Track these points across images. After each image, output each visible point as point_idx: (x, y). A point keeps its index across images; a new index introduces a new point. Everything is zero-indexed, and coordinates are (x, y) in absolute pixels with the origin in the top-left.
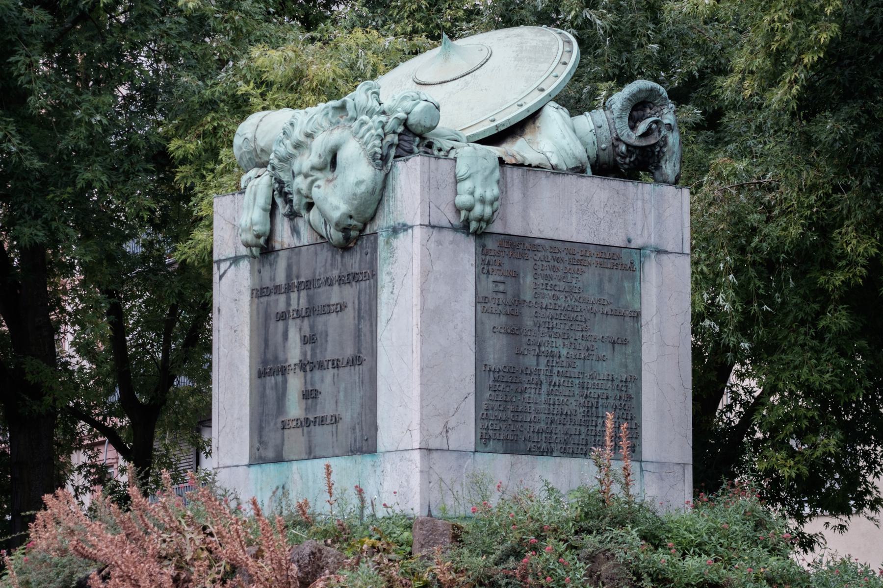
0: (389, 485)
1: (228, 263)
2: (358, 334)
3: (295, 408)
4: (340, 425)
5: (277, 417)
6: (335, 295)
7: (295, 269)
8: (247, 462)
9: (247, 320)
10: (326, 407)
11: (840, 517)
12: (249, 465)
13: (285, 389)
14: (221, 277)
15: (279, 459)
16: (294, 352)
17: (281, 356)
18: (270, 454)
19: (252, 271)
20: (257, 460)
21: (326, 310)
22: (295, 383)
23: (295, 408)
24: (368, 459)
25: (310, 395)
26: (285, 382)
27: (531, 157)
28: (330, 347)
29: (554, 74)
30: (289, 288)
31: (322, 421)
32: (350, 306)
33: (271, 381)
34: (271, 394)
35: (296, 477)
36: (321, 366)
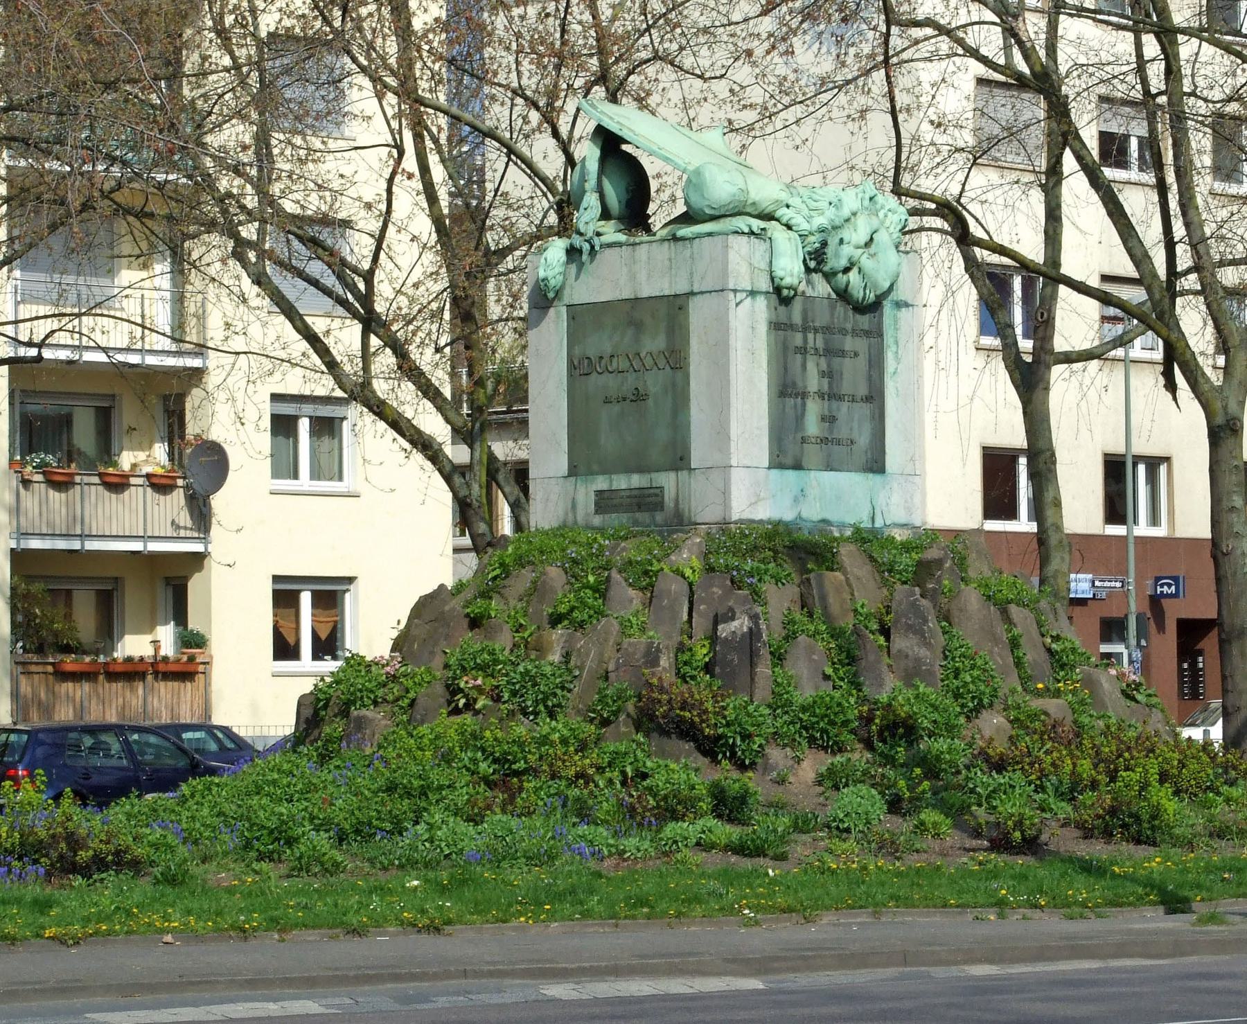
0: (896, 499)
1: (745, 294)
2: (870, 379)
3: (812, 426)
4: (854, 447)
5: (796, 432)
6: (849, 343)
7: (810, 314)
8: (767, 464)
9: (765, 346)
10: (842, 432)
11: (649, 212)
12: (769, 468)
13: (804, 410)
14: (737, 305)
15: (798, 466)
16: (813, 382)
17: (800, 384)
18: (789, 460)
19: (768, 307)
20: (777, 463)
21: (842, 353)
22: (813, 409)
23: (812, 426)
24: (877, 478)
25: (829, 419)
26: (804, 405)
27: (54, 342)
28: (845, 384)
29: (248, 443)
30: (805, 330)
31: (839, 442)
32: (861, 355)
33: (790, 402)
34: (790, 412)
35: (814, 483)
36: (840, 398)
